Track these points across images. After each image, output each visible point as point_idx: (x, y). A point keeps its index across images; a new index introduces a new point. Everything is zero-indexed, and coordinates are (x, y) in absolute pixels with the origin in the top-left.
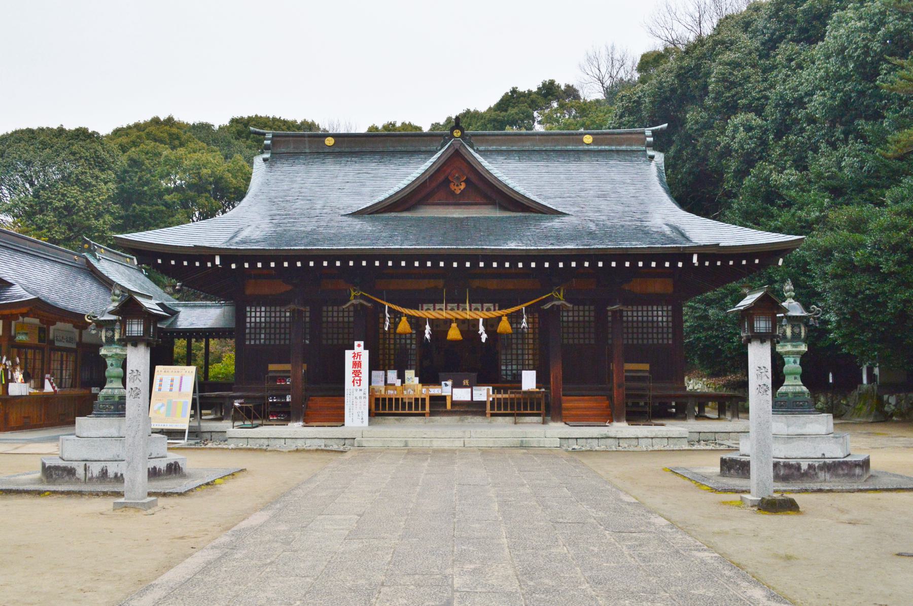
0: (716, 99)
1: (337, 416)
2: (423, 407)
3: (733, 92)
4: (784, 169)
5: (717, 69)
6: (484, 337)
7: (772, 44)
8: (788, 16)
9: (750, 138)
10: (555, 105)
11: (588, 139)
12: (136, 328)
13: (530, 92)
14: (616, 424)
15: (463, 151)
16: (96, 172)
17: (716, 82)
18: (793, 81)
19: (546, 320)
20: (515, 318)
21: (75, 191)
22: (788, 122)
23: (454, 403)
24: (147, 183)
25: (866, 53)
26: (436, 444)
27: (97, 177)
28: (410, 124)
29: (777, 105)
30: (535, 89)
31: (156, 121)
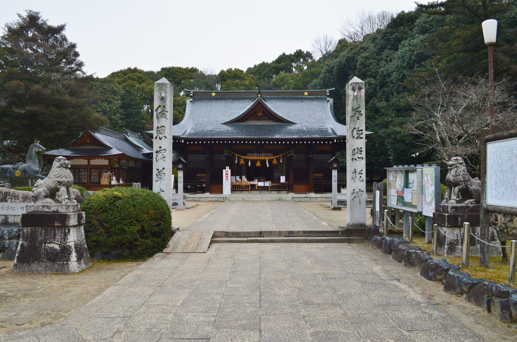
0: (359, 72)
1: (221, 191)
2: (248, 188)
3: (366, 69)
4: (382, 101)
5: (360, 60)
6: (268, 165)
7: (382, 50)
8: (388, 39)
9: (371, 88)
10: (302, 60)
11: (306, 94)
12: (180, 166)
13: (291, 54)
14: (311, 193)
15: (261, 102)
16: (113, 96)
17: (360, 65)
18: (387, 67)
19: (289, 160)
20: (278, 160)
21: (106, 104)
22: (385, 82)
23: (258, 187)
24: (133, 100)
25: (410, 60)
26: (253, 199)
27: (114, 98)
28: (238, 69)
29: (381, 76)
30: (293, 54)
31: (129, 69)
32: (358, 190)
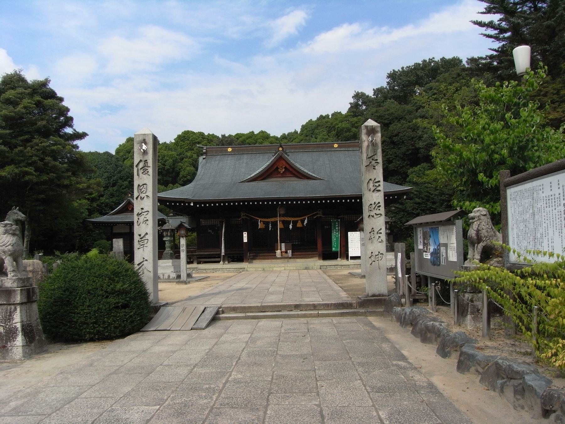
15: (283, 156)
32: (377, 253)
